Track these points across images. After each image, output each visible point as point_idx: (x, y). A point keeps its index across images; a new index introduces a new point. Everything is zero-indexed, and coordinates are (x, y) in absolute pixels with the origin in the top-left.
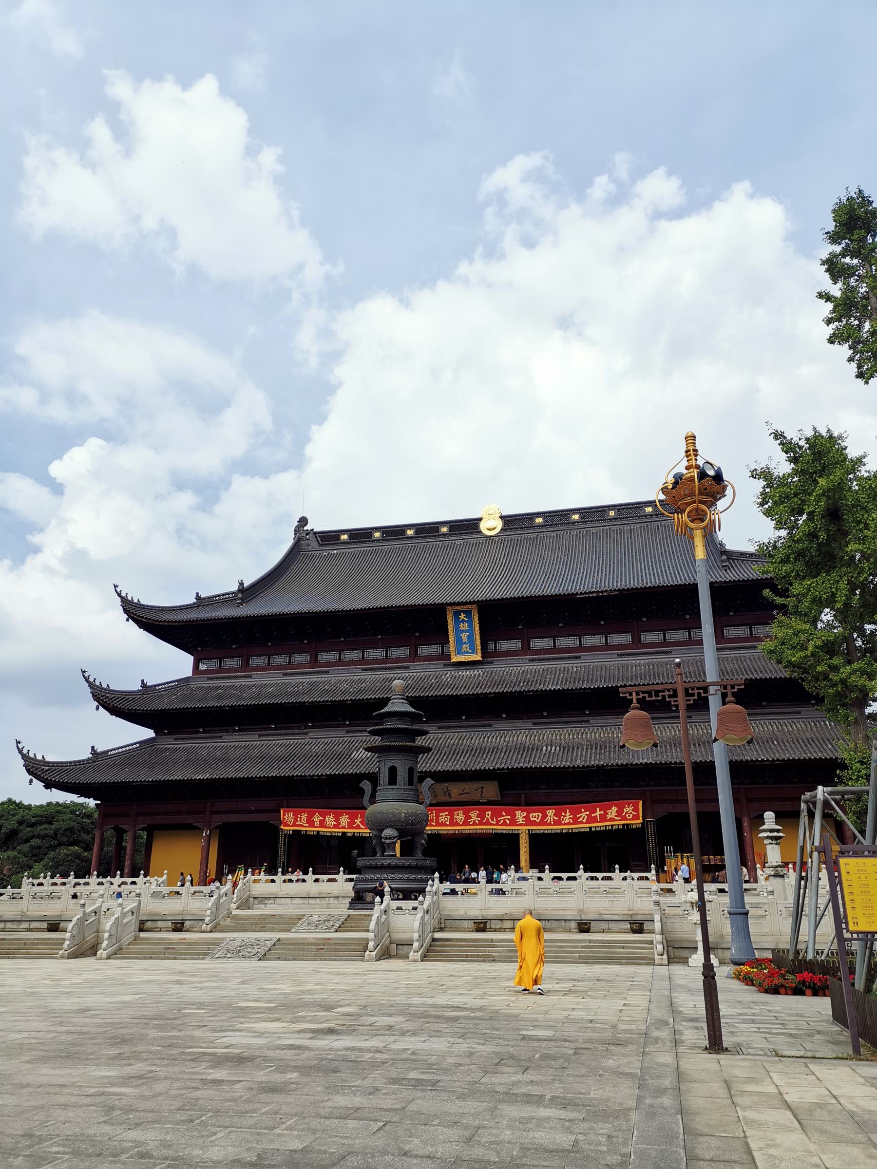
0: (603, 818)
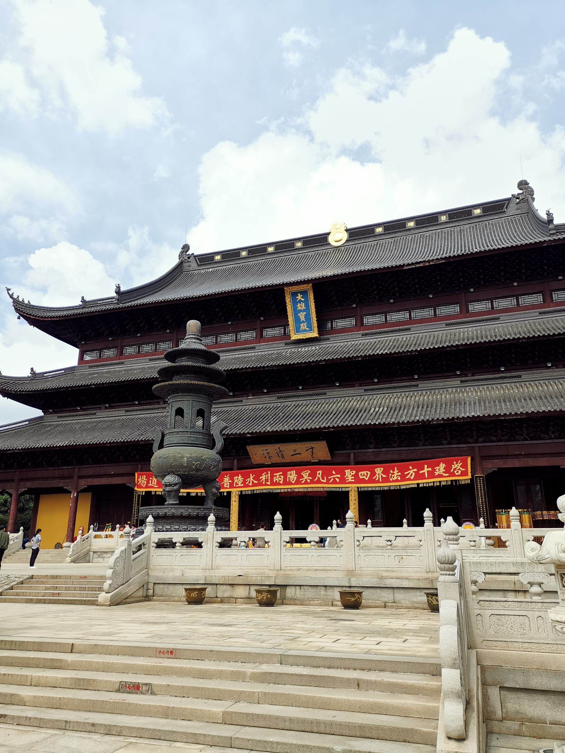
0: (431, 475)
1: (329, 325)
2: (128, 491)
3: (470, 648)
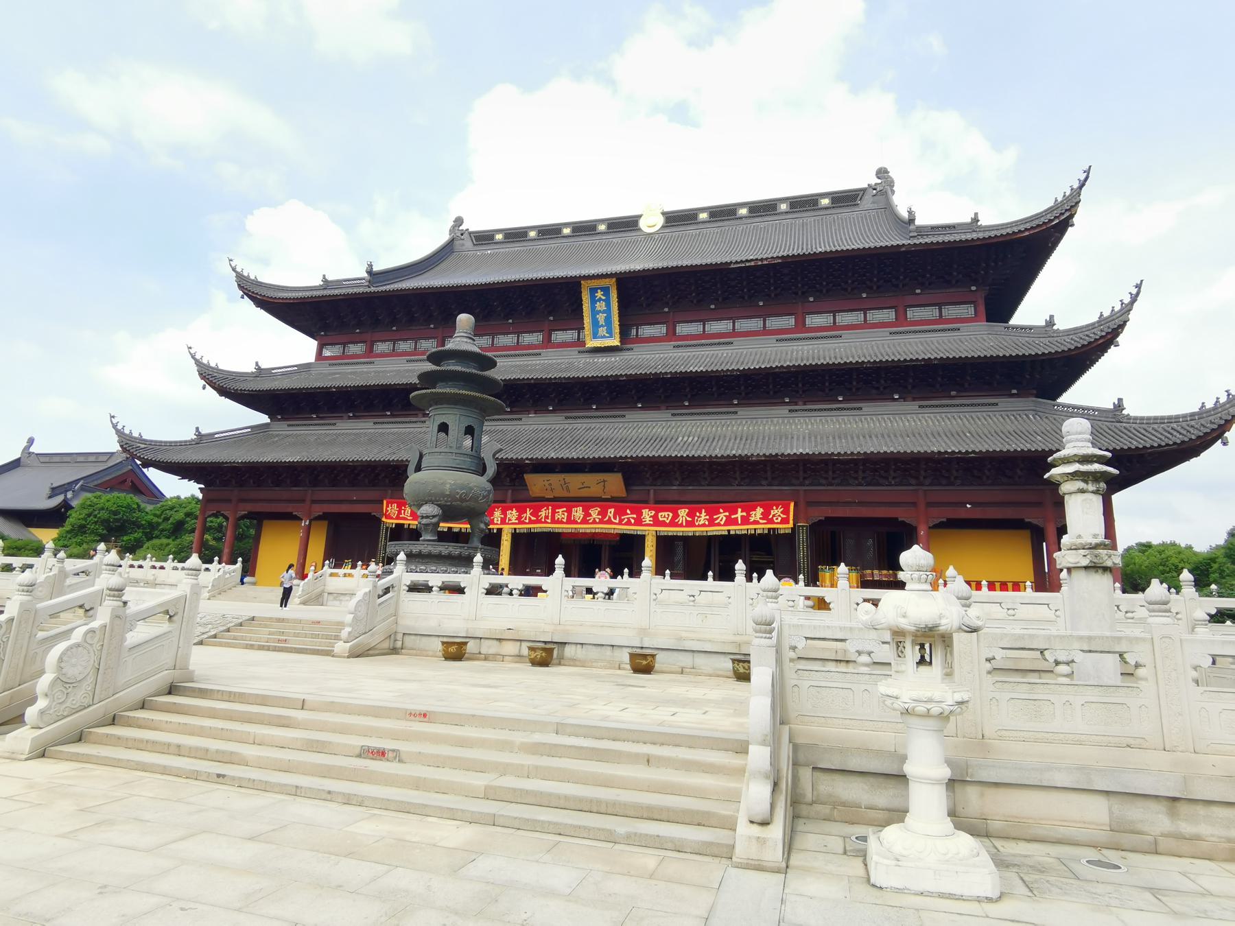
0: (745, 520)
1: (634, 332)
2: (373, 522)
3: (782, 723)
